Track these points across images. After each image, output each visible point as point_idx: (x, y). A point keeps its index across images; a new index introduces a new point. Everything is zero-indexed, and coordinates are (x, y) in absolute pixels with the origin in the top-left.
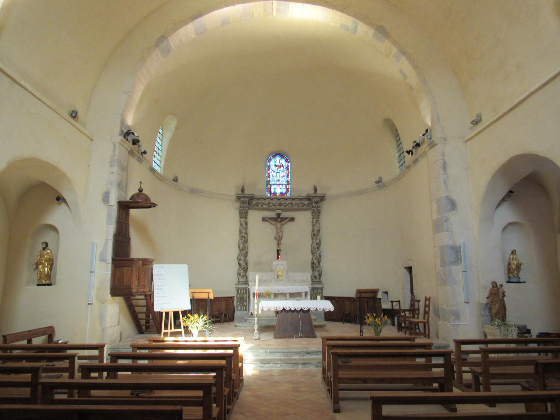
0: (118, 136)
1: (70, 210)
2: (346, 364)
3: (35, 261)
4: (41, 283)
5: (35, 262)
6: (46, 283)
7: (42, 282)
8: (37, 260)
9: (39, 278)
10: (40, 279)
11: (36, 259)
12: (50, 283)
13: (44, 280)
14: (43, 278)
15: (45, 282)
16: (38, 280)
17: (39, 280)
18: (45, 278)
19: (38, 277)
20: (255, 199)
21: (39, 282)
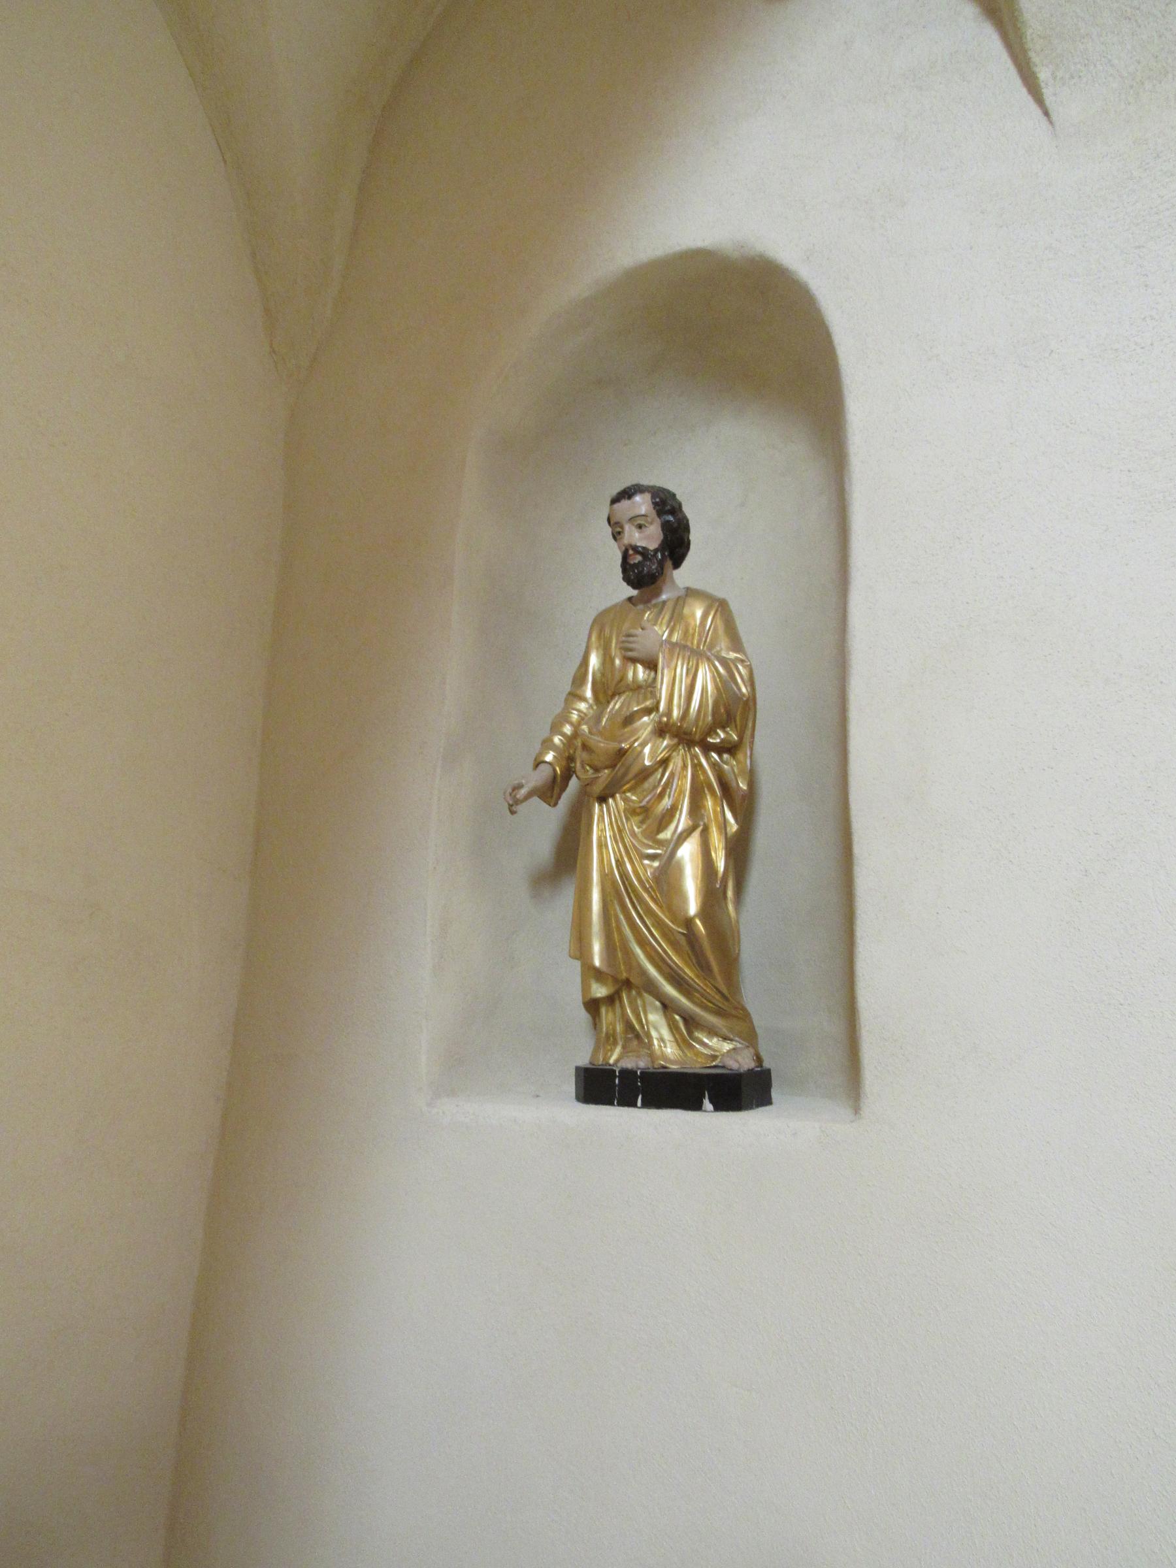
0: (712, 1112)
1: (1046, 113)
2: (702, 644)
3: (547, 744)
4: (637, 1063)
5: (538, 763)
6: (696, 1066)
7: (636, 1036)
8: (570, 740)
9: (600, 991)
10: (611, 1000)
11: (555, 728)
12: (744, 1062)
13: (667, 1006)
14: (651, 988)
15: (683, 1043)
16: (593, 1006)
17: (607, 1016)
18: (670, 990)
19: (591, 973)
20: (724, 781)
21: (610, 1039)
